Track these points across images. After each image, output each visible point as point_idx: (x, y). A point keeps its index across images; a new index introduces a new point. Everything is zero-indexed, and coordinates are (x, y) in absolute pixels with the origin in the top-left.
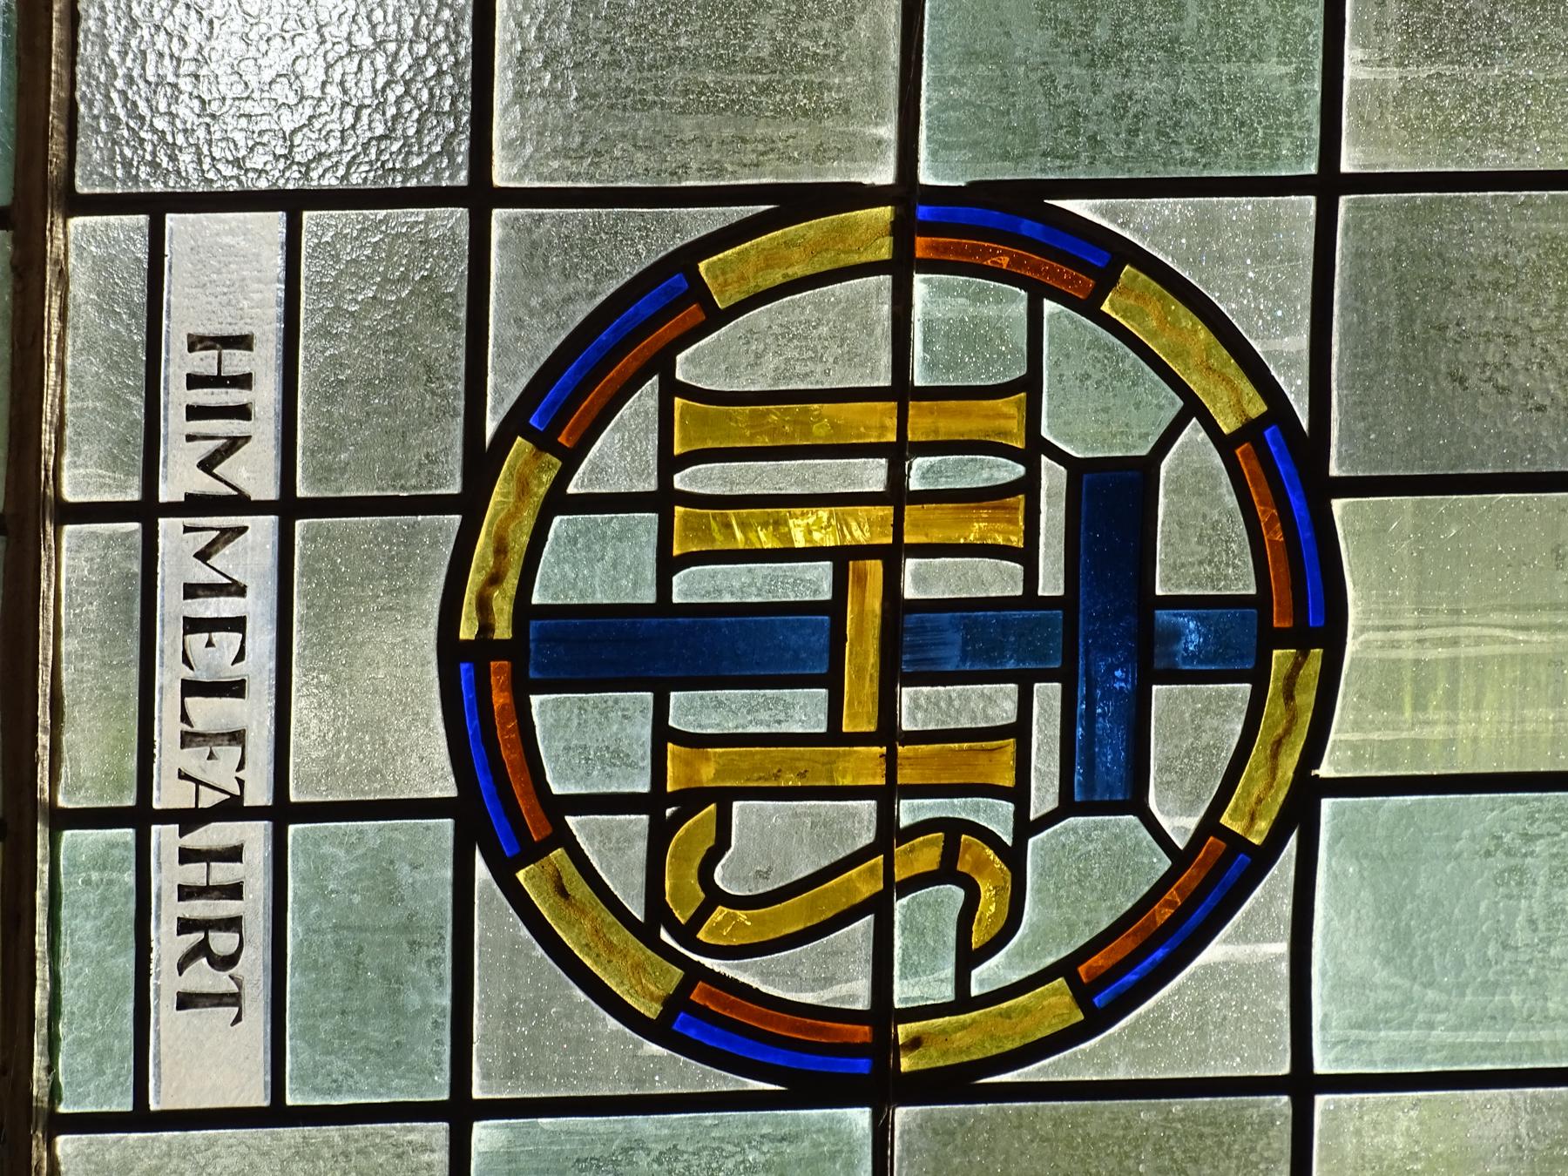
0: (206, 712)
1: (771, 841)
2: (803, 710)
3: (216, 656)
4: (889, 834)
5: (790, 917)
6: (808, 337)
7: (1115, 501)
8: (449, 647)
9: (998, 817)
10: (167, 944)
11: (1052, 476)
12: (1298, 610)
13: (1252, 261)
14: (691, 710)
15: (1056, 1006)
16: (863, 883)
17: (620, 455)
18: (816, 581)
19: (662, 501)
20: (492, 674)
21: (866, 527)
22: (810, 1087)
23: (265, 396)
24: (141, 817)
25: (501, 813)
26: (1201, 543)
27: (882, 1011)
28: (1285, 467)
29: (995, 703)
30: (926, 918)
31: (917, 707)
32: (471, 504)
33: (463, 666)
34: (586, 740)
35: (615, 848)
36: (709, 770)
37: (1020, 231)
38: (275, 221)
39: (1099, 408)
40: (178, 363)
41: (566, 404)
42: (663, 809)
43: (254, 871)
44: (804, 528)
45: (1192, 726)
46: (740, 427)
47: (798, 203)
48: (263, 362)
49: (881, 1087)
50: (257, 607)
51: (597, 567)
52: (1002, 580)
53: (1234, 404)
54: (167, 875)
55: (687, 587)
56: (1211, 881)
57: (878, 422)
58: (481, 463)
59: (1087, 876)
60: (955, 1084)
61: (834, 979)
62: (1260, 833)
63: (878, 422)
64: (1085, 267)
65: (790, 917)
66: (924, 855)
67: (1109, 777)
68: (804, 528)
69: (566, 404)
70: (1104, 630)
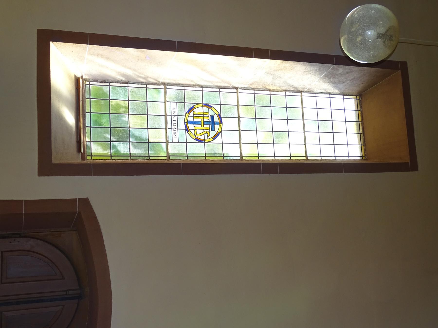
0: (174, 124)
1: (199, 132)
2: (200, 126)
3: (174, 122)
4: (204, 131)
5: (200, 135)
6: (199, 110)
7: (213, 117)
8: (185, 123)
9: (209, 131)
10: (173, 135)
11: (210, 116)
12: (221, 122)
13: (217, 107)
14: (195, 125)
15: (212, 139)
16: (203, 133)
17: (191, 114)
18: (200, 120)
19: (193, 116)
20: (187, 123)
21: (202, 118)
22: (203, 142)
23: (176, 111)
24: (172, 129)
25: (187, 130)
26: (216, 119)
27: (204, 139)
28: (220, 116)
29: (208, 126)
30: (206, 135)
31: (205, 126)
32: (185, 116)
33: (299, 114)
34: (191, 126)
35: (192, 131)
36: (196, 128)
37: (207, 105)
38: (237, 117)
39: (211, 113)
40: (172, 109)
41: (189, 112)
42: (194, 130)
43: (177, 131)
44: (200, 118)
45: (216, 127)
46: (197, 113)
47: (198, 104)
48: (176, 109)
49: (205, 142)
50: (176, 120)
51: (191, 119)
52: (208, 120)
53: (217, 114)
54: (173, 132)
55: (195, 120)
56: (218, 134)
57: (202, 113)
58: (185, 114)
59: (213, 134)
60: (207, 142)
61: (202, 137)
62: (364, 45)
63: (202, 113)
64: (211, 107)
65: (200, 135)
66: (205, 132)
67: (213, 129)
68: (200, 118)
69: (189, 112)
70: (213, 123)
